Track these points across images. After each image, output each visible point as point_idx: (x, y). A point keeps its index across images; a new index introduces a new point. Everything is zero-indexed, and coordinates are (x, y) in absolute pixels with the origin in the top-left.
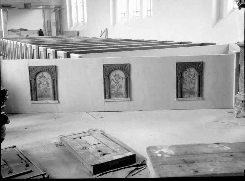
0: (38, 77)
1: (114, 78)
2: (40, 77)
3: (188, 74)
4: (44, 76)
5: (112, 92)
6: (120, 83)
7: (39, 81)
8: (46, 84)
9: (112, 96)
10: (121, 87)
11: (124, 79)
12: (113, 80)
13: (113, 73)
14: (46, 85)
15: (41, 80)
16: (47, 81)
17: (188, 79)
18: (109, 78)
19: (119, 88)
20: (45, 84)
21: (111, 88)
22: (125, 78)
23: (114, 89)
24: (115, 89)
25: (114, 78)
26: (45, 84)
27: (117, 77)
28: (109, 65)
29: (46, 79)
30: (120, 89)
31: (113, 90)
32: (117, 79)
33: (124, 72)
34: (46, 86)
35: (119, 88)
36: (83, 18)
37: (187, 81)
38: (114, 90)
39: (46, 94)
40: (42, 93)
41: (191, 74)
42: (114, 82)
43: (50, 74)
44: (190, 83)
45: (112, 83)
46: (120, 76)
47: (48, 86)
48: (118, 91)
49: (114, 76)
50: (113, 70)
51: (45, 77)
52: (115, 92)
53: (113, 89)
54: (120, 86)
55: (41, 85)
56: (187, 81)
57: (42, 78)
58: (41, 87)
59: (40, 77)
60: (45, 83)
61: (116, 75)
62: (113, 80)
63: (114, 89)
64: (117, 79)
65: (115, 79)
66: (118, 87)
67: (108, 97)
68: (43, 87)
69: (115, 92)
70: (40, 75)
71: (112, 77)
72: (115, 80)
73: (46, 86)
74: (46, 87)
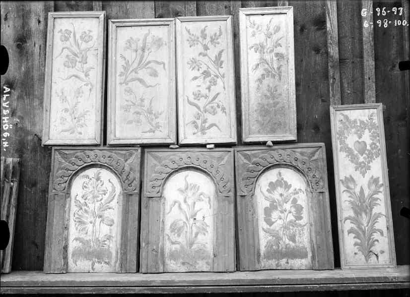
2: (271, 184)
3: (91, 189)
4: (286, 182)
8: (293, 210)
15: (276, 195)
17: (91, 206)
19: (197, 234)
25: (181, 198)
27: (190, 193)
32: (190, 202)
34: (291, 217)
36: (342, 38)
37: (86, 211)
40: (278, 244)
41: (103, 188)
43: (122, 182)
44: (98, 220)
47: (300, 218)
48: (191, 244)
51: (287, 187)
55: (275, 215)
56: (86, 211)
57: (279, 188)
60: (288, 206)
61: (187, 189)
63: (179, 236)
64: (190, 202)
65: (185, 201)
68: (280, 222)
69: (182, 247)
72: (184, 206)
73: (291, 217)
74: (291, 222)
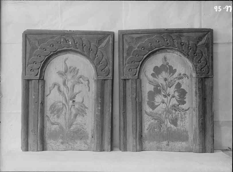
0: (149, 67)
1: (60, 80)
4: (171, 67)
5: (50, 128)
6: (78, 99)
7: (150, 82)
8: (176, 94)
9: (50, 142)
10: (83, 111)
11: (93, 86)
12: (56, 87)
13: (57, 64)
14: (173, 97)
15: (160, 79)
16: (179, 85)
18: (42, 79)
19: (76, 116)
20: (172, 93)
21: (48, 112)
22: (97, 81)
23: (58, 117)
24: (62, 117)
26: (172, 93)
27: (69, 77)
28: (44, 37)
29: (176, 75)
30: (79, 119)
31: (54, 123)
33: (88, 57)
34: (174, 102)
35: (76, 116)
38: (59, 121)
39: (175, 128)
42: (57, 93)
45: (53, 97)
46: (79, 74)
49: (60, 74)
50: (57, 53)
51: (172, 71)
52: (61, 127)
53: (53, 118)
54: (78, 110)
58: (156, 104)
59: (157, 71)
62: (56, 87)
63: (58, 117)
64: (69, 84)
65: (64, 84)
66: (74, 111)
67: (131, 147)
68: (163, 106)
70: (157, 60)
71: (53, 73)
72: (62, 87)
73: (174, 102)
74: (174, 106)
